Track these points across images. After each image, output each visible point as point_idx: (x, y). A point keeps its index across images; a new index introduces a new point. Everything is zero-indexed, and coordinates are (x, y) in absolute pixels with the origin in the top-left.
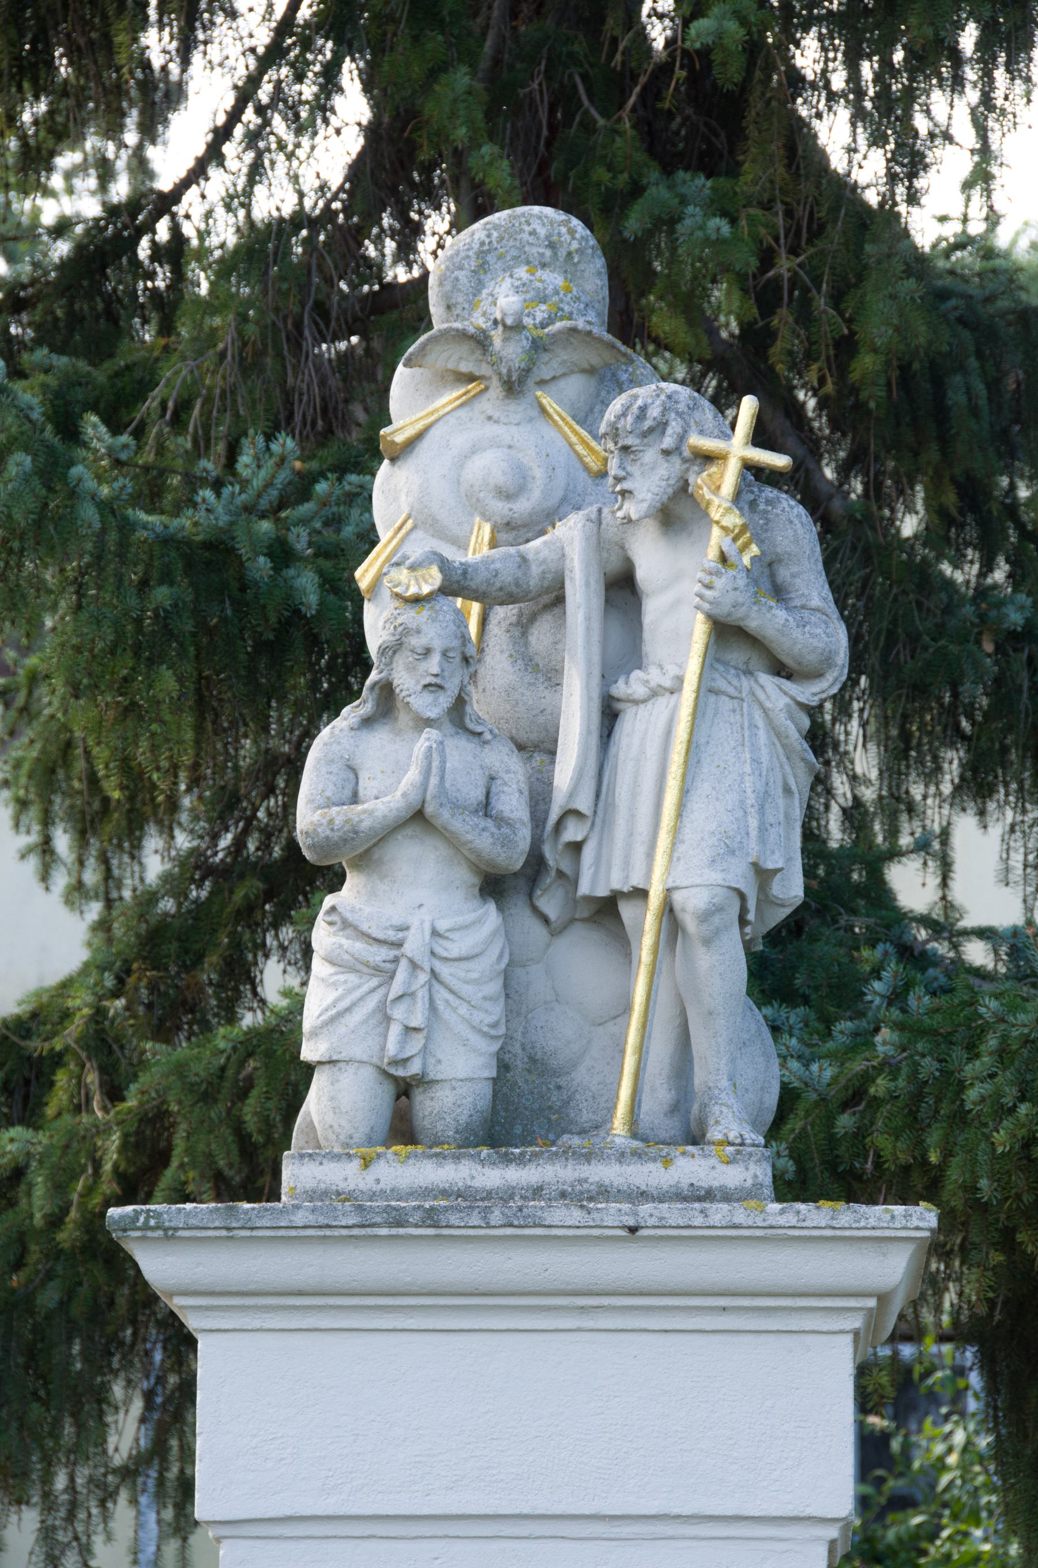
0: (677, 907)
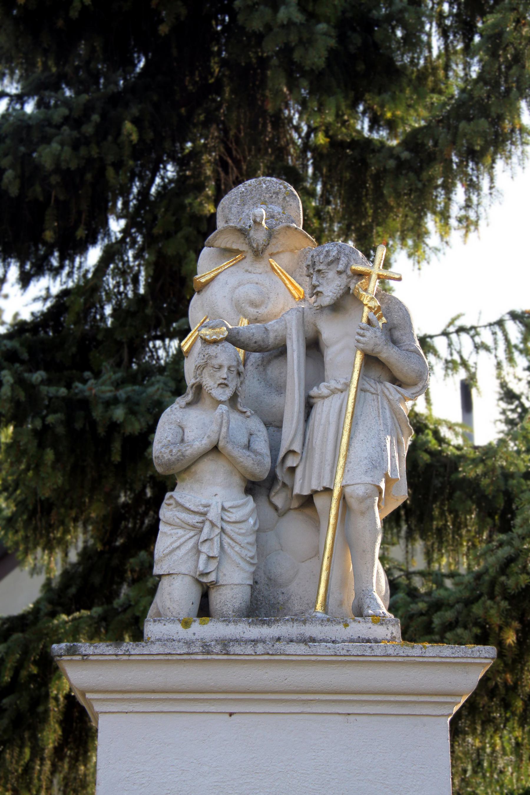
0: (347, 496)
